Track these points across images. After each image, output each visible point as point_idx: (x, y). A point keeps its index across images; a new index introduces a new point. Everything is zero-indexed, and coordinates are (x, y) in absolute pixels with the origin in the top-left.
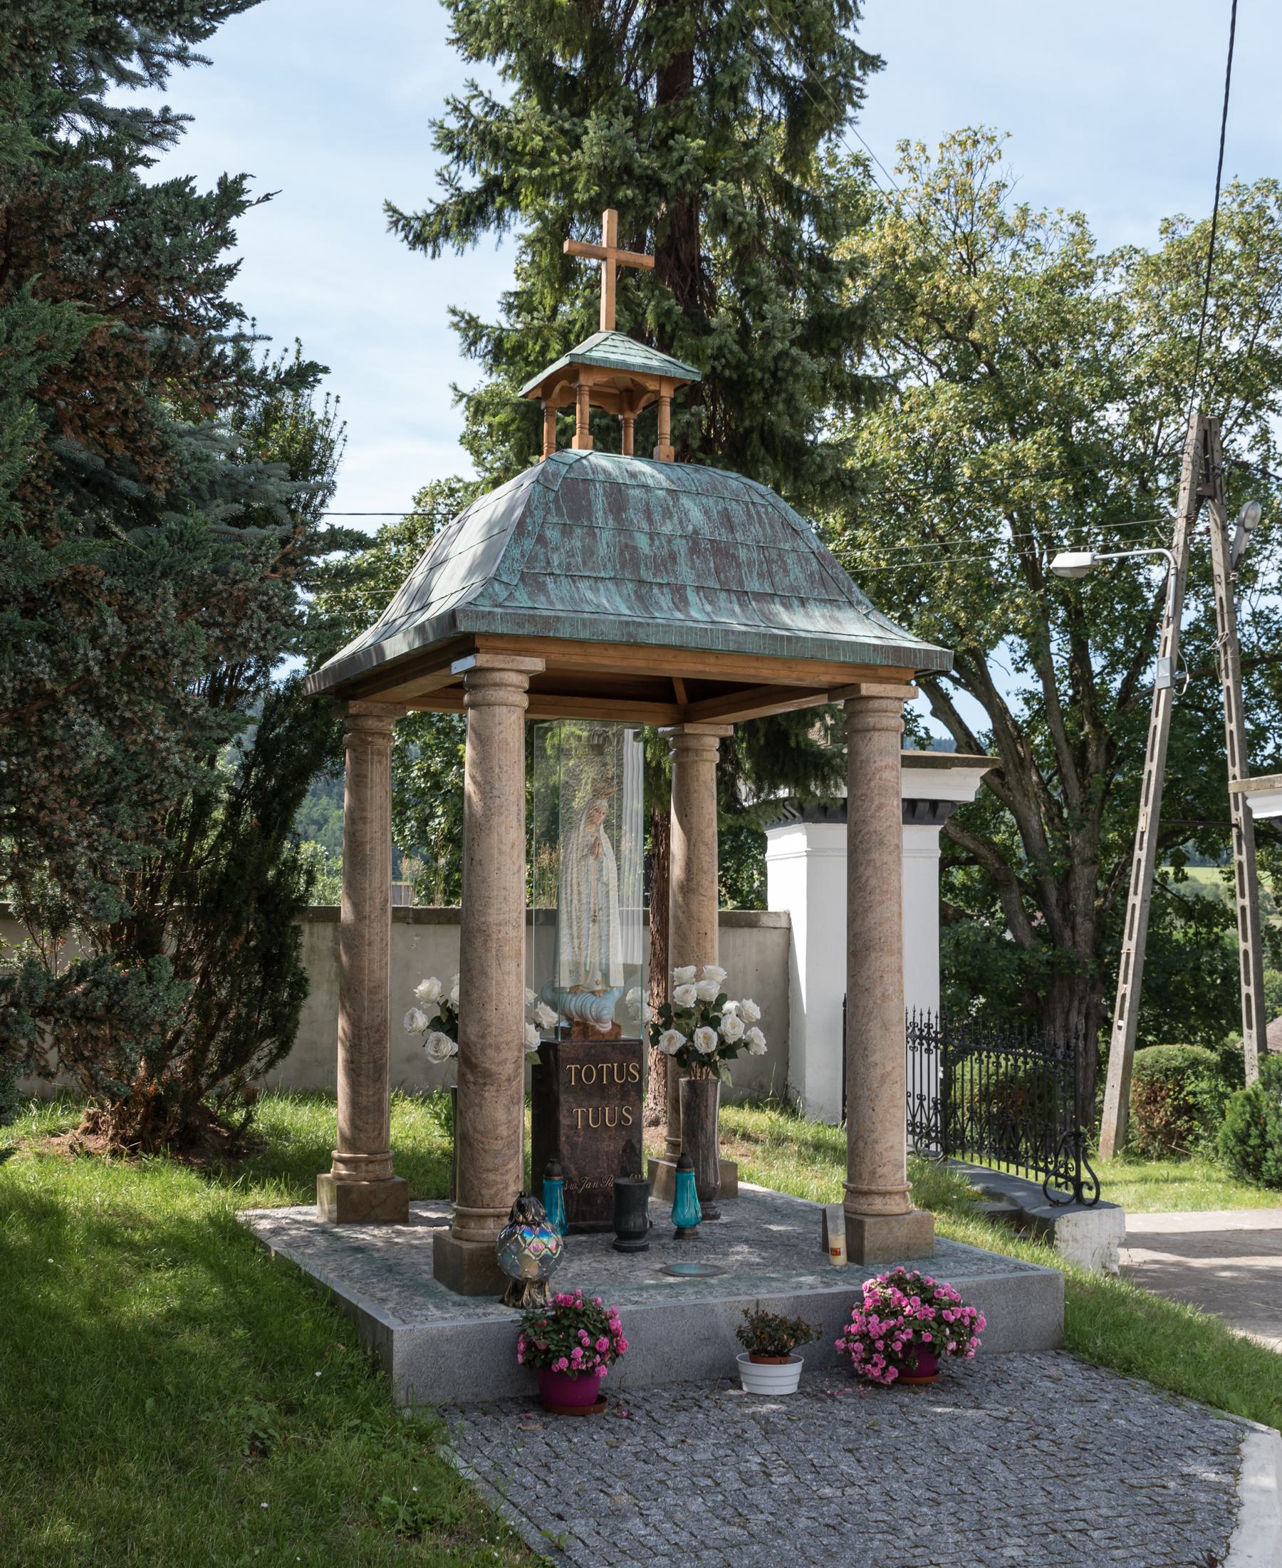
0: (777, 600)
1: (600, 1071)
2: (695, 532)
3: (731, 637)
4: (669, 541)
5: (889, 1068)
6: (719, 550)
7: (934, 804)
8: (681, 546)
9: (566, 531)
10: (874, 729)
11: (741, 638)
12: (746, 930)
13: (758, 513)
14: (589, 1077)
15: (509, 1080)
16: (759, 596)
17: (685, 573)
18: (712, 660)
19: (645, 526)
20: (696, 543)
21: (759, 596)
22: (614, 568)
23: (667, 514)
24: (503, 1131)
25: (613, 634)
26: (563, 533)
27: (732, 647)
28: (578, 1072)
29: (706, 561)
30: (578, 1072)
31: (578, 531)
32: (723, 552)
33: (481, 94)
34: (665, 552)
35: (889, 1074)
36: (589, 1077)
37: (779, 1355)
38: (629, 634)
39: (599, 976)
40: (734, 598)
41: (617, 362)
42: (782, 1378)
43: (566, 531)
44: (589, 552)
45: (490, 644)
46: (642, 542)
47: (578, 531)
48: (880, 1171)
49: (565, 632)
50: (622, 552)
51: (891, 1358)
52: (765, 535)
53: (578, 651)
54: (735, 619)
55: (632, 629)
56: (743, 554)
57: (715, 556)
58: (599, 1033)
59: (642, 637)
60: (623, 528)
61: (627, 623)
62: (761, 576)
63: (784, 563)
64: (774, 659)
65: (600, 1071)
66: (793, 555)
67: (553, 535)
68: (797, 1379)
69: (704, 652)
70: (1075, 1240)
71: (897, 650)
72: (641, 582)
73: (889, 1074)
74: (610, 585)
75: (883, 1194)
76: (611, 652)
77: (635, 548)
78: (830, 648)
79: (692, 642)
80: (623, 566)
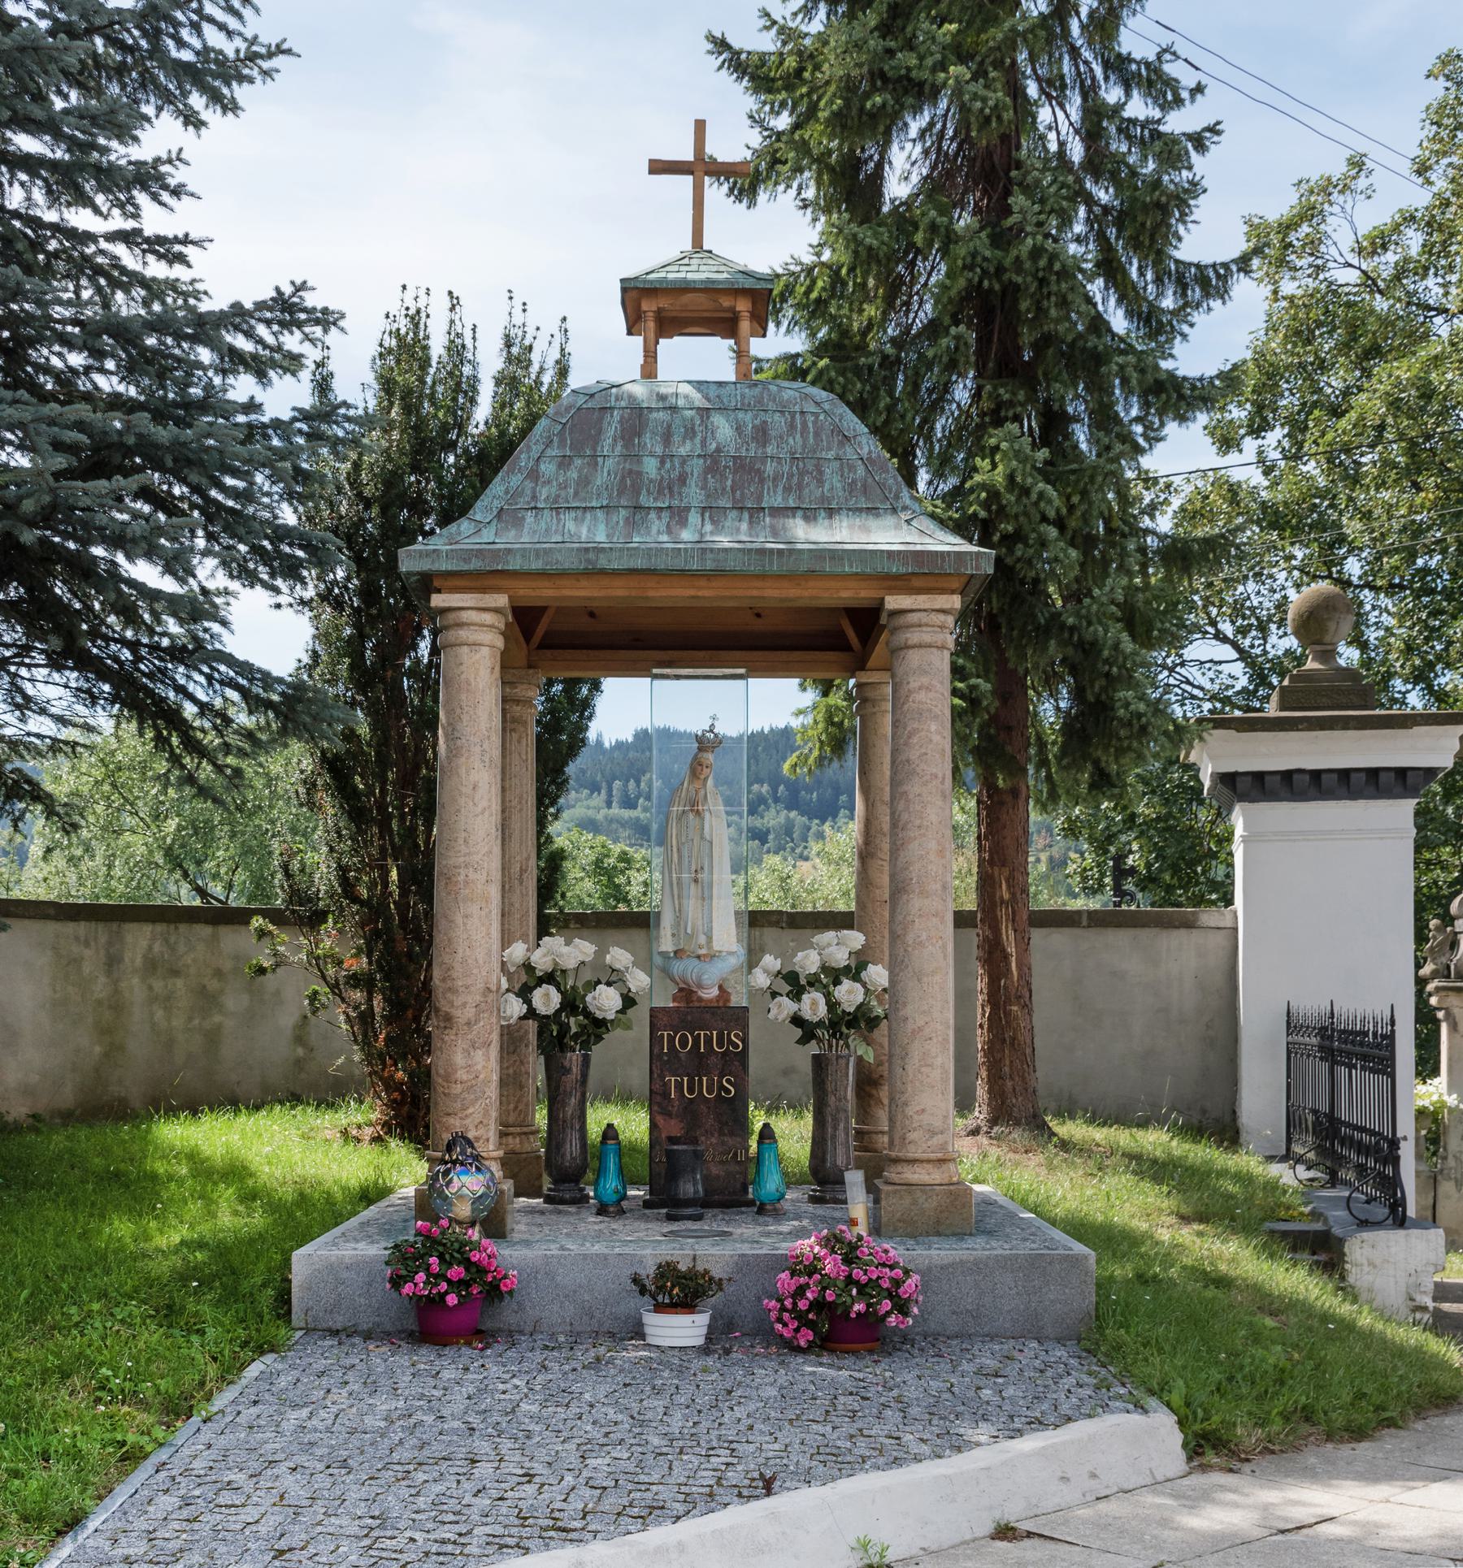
0: (800, 513)
1: (697, 1040)
2: (718, 450)
3: (709, 556)
4: (683, 463)
5: (921, 1023)
6: (742, 466)
7: (1401, 773)
8: (696, 466)
9: (564, 462)
10: (908, 647)
11: (722, 556)
12: (1183, 932)
13: (804, 424)
14: (684, 1044)
15: (468, 1024)
16: (776, 512)
17: (694, 494)
18: (703, 582)
19: (659, 450)
20: (716, 462)
21: (776, 512)
22: (610, 497)
23: (690, 433)
24: (461, 1075)
25: (570, 563)
26: (560, 466)
27: (709, 565)
28: (671, 1039)
29: (724, 478)
30: (671, 1039)
31: (578, 462)
32: (747, 469)
33: (774, 23)
34: (675, 474)
35: (920, 1029)
36: (684, 1044)
37: (685, 1304)
38: (588, 561)
39: (702, 940)
40: (746, 515)
41: (675, 281)
42: (681, 1330)
43: (564, 462)
44: (584, 482)
45: (451, 583)
46: (650, 466)
47: (578, 462)
48: (912, 1136)
49: (515, 564)
50: (623, 478)
51: (800, 1317)
52: (804, 446)
53: (546, 584)
54: (729, 537)
55: (591, 556)
56: (770, 468)
57: (735, 472)
58: (700, 999)
59: (603, 562)
60: (632, 455)
61: (587, 550)
62: (788, 490)
63: (821, 473)
64: (762, 577)
65: (697, 1040)
66: (836, 464)
67: (547, 468)
68: (704, 1331)
69: (683, 574)
70: (1371, 1264)
71: (919, 556)
72: (638, 508)
73: (920, 1029)
74: (600, 514)
75: (914, 1161)
76: (584, 583)
77: (640, 473)
78: (832, 558)
79: (661, 564)
80: (621, 493)
